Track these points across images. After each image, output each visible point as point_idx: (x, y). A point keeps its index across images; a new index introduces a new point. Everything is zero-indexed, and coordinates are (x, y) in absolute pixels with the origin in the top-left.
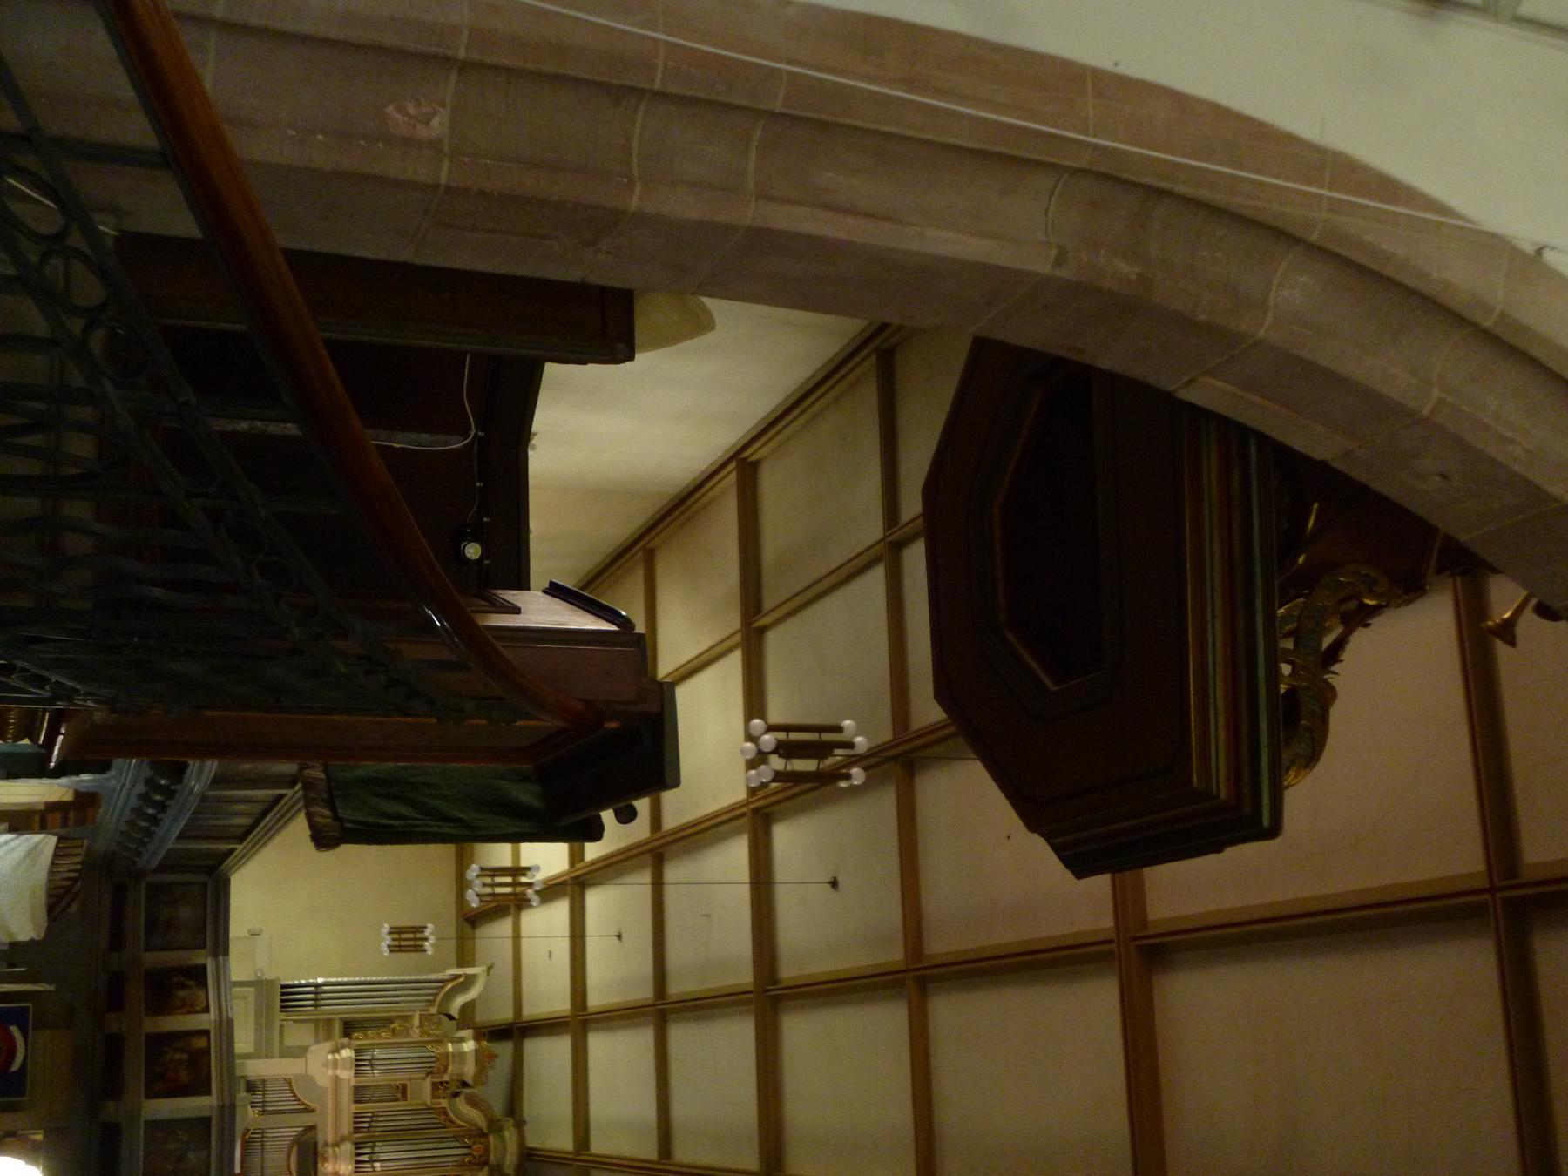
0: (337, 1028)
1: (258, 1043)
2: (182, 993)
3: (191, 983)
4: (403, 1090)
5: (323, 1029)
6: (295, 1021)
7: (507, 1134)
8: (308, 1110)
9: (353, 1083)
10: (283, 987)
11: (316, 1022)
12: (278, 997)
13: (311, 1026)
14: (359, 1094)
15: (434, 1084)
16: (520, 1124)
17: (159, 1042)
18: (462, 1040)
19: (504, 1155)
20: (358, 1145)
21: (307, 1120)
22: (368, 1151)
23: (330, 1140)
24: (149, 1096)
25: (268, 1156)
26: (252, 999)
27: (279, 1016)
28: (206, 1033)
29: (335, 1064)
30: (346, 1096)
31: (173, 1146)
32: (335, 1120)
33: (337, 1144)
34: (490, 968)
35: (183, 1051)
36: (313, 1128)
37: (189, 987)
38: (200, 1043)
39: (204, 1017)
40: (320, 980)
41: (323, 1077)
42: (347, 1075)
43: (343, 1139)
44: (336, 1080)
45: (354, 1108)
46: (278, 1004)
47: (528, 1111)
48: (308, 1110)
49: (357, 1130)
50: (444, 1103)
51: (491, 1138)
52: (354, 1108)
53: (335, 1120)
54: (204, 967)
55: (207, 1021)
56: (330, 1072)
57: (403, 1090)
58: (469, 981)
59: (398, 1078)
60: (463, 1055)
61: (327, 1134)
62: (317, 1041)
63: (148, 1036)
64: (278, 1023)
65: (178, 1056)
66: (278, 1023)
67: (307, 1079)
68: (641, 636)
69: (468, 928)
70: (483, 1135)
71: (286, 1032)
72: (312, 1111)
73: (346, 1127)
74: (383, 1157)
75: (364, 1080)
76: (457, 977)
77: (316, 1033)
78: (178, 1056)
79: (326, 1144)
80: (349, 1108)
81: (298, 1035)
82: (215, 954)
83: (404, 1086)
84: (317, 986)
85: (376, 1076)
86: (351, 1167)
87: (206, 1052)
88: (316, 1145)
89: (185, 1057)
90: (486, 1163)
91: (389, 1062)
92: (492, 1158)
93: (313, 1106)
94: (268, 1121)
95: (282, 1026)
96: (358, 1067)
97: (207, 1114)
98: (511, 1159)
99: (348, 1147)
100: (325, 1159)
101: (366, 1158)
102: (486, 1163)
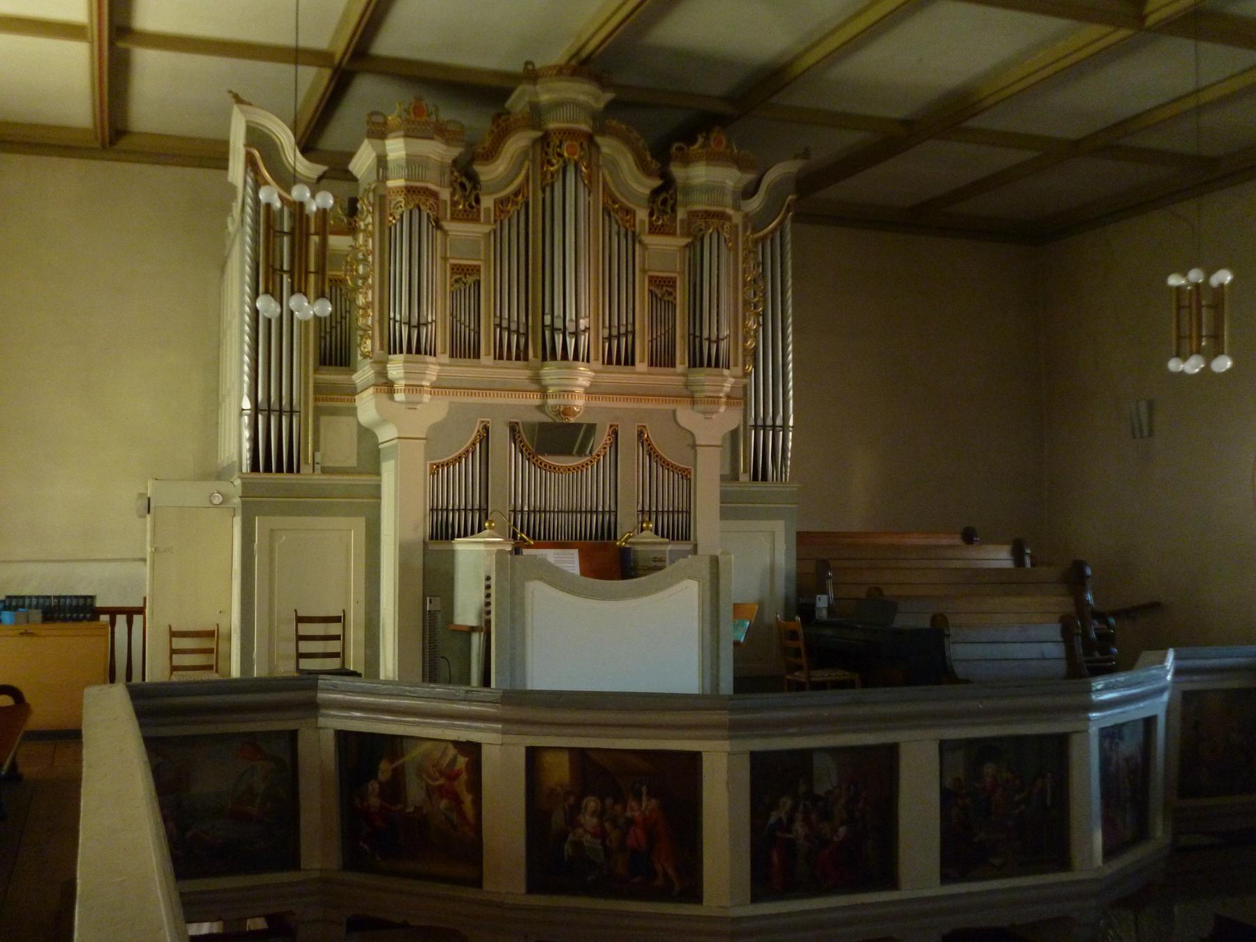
0: (332, 376)
1: (350, 511)
2: (415, 792)
3: (385, 769)
4: (460, 271)
5: (336, 400)
6: (316, 449)
7: (545, 98)
8: (485, 437)
9: (445, 358)
10: (255, 467)
11: (318, 412)
12: (274, 476)
13: (324, 419)
14: (464, 348)
15: (454, 218)
16: (531, 75)
17: (550, 863)
18: (382, 161)
19: (576, 104)
20: (548, 354)
21: (500, 440)
22: (559, 339)
23: (536, 401)
24: (693, 893)
25: (551, 505)
26: (277, 521)
27: (307, 475)
28: (533, 755)
29: (413, 388)
30: (466, 371)
31: (799, 828)
32: (505, 392)
33: (543, 391)
34: (238, 100)
35: (576, 809)
36: (513, 428)
37: (398, 774)
38: (559, 772)
39: (490, 757)
40: (247, 404)
41: (434, 409)
42: (433, 369)
43: (536, 379)
44: (436, 387)
45: (486, 359)
46: (285, 476)
47: (486, 56)
48: (485, 437)
49: (522, 355)
50: (487, 202)
51: (552, 126)
52: (486, 359)
53: (505, 392)
54: (343, 737)
55: (503, 756)
56: (426, 398)
57: (460, 271)
58: (258, 139)
59: (438, 279)
60: (412, 162)
61: (525, 406)
62: (353, 412)
63: (533, 887)
64: (319, 478)
65: (589, 821)
66: (319, 478)
67: (435, 435)
68: (98, 619)
69: (123, 143)
70: (545, 140)
71: (329, 464)
72: (486, 429)
73: (516, 373)
74: (570, 314)
75: (441, 340)
76: (250, 162)
77: (334, 412)
78: (589, 821)
79: (541, 408)
80: (486, 368)
81: (338, 444)
82: (312, 707)
83: (456, 269)
84: (256, 409)
85: (437, 317)
86: (582, 368)
87: (580, 757)
88: (543, 426)
89: (591, 803)
90: (590, 138)
91: (416, 296)
92: (584, 127)
93: (478, 427)
94: (499, 505)
95: (324, 471)
96: (418, 349)
97: (745, 763)
98: (584, 93)
99: (551, 372)
100: (567, 411)
101: (571, 343)
102: (590, 138)
